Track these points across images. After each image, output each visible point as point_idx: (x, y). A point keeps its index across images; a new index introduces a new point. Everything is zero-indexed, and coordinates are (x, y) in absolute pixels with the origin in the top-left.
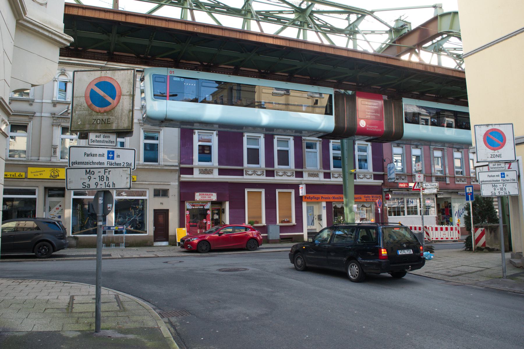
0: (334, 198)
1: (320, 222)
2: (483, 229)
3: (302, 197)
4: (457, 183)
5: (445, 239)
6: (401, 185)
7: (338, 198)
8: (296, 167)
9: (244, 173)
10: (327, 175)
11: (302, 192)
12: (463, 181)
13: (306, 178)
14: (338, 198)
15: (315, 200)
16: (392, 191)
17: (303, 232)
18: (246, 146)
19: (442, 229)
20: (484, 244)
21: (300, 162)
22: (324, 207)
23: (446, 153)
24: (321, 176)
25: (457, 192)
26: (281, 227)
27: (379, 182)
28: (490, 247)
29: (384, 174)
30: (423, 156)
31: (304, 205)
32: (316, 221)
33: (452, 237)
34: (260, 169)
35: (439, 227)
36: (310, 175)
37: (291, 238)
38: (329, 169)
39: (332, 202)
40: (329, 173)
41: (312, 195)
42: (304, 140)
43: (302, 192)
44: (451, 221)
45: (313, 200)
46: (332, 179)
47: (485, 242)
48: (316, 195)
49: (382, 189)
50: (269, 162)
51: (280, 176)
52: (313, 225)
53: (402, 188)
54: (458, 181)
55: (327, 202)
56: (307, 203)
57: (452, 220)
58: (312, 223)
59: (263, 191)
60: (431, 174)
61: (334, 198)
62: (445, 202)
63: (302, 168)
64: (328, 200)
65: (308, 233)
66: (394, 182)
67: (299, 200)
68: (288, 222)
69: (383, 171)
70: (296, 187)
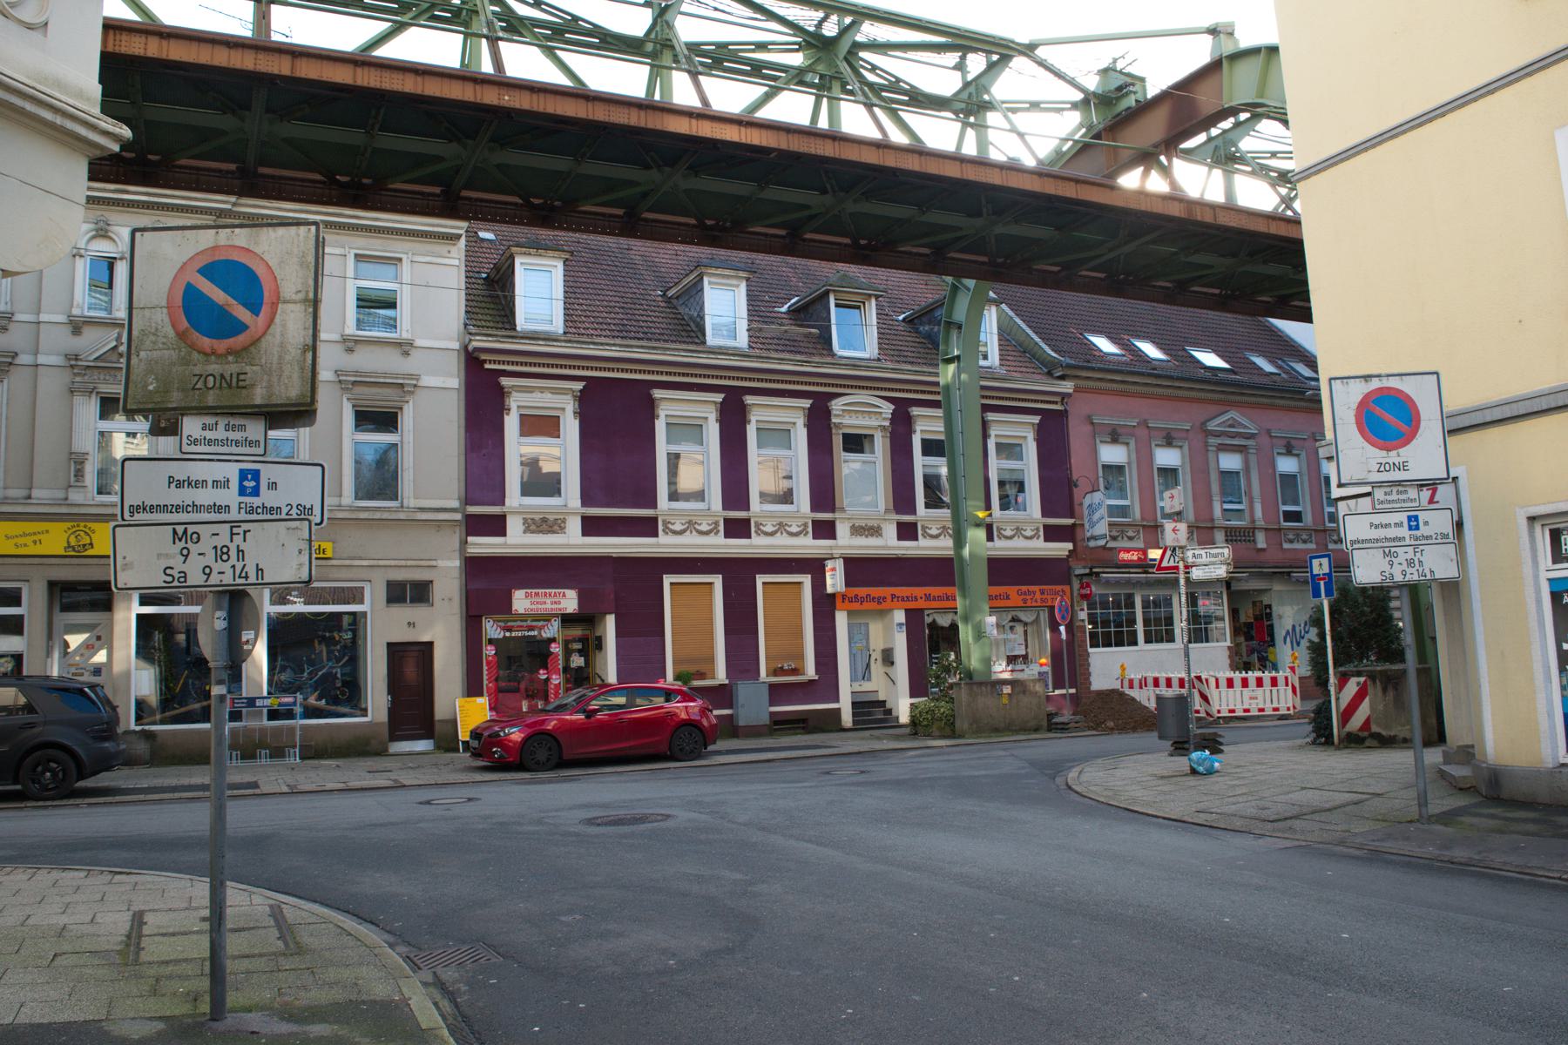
0: (928, 597)
2: (1362, 679)
3: (833, 596)
4: (1286, 546)
5: (1254, 713)
6: (1124, 556)
7: (940, 598)
8: (816, 505)
9: (660, 527)
10: (907, 531)
12: (1305, 542)
14: (940, 598)
17: (837, 700)
19: (1245, 683)
21: (824, 492)
22: (900, 625)
23: (1253, 459)
24: (890, 531)
25: (1289, 573)
27: (1061, 549)
31: (841, 619)
32: (877, 669)
33: (1275, 705)
35: (1237, 676)
36: (857, 531)
37: (804, 721)
38: (913, 511)
39: (922, 610)
40: (914, 525)
41: (862, 591)
42: (838, 426)
43: (835, 581)
44: (1271, 657)
45: (866, 606)
46: (923, 542)
49: (1070, 568)
51: (766, 534)
52: (869, 679)
53: (1127, 565)
54: (1291, 541)
55: (908, 611)
56: (850, 614)
58: (866, 674)
59: (717, 581)
60: (1212, 520)
63: (833, 510)
64: (912, 605)
67: (825, 606)
68: (795, 671)
69: (1072, 516)
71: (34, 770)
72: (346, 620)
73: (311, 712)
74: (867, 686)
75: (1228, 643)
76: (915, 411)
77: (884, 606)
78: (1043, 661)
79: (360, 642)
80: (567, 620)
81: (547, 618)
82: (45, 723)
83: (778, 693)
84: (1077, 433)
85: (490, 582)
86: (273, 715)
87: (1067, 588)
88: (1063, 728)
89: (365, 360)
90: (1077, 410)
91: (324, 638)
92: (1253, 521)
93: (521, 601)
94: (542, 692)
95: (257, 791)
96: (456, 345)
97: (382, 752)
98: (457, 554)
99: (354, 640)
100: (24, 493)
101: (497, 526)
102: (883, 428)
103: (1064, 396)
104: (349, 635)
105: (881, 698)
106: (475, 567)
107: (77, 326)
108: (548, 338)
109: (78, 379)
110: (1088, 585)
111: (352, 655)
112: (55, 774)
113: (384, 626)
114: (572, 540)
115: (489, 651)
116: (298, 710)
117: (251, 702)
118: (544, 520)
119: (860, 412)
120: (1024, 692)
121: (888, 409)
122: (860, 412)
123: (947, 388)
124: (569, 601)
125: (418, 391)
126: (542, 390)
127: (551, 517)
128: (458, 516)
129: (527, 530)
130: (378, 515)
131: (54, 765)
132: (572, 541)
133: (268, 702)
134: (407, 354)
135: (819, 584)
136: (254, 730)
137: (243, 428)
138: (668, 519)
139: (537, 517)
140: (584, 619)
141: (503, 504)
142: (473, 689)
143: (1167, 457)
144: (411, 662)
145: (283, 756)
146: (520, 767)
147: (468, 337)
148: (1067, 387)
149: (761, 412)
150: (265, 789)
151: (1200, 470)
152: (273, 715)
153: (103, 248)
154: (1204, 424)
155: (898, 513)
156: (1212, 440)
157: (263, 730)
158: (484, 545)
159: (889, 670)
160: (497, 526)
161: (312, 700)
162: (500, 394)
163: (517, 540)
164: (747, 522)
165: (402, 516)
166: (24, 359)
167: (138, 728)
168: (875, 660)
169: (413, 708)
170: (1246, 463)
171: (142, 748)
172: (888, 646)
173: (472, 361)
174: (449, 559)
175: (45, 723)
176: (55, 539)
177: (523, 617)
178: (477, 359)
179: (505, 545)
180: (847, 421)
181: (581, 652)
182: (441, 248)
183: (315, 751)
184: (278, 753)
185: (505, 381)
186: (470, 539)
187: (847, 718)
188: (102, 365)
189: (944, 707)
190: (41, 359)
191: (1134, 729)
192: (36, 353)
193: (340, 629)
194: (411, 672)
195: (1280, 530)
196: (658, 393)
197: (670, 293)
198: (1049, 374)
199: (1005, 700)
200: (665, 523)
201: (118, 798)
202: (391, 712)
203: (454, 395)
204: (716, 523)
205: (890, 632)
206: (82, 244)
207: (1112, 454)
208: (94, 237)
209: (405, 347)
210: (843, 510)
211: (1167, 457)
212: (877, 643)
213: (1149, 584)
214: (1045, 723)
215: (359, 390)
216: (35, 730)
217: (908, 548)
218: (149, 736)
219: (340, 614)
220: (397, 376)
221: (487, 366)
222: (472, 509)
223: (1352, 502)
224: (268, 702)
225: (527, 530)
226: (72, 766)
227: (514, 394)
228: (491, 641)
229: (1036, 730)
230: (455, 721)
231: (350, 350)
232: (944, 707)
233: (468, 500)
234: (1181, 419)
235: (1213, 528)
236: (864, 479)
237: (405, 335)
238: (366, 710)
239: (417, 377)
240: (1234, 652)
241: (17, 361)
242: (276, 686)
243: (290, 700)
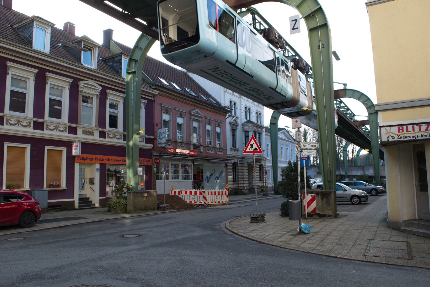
0: (108, 160)
1: (92, 186)
2: (313, 195)
3: (75, 156)
4: (207, 151)
5: (217, 203)
6: (170, 150)
7: (112, 160)
8: (70, 121)
9: (5, 121)
10: (102, 135)
11: (76, 151)
13: (80, 135)
14: (112, 160)
15: (89, 161)
16: (162, 156)
17: (73, 198)
18: (9, 88)
20: (314, 210)
22: (98, 169)
23: (201, 124)
24: (97, 134)
25: (209, 160)
26: (49, 192)
27: (150, 146)
28: (321, 213)
29: (154, 139)
30: (185, 124)
31: (77, 166)
32: (87, 186)
33: (212, 201)
34: (27, 118)
36: (85, 132)
37: (60, 206)
38: (105, 127)
39: (106, 164)
41: (85, 156)
42: (82, 91)
43: (76, 151)
44: (202, 185)
46: (107, 139)
47: (315, 208)
48: (90, 156)
49: (152, 153)
50: (39, 111)
51: (50, 130)
52: (84, 189)
53: (171, 153)
54: (208, 150)
55: (101, 164)
56: (80, 164)
57: (203, 184)
59: (28, 147)
60: (190, 142)
61: (108, 160)
62: (197, 168)
63: (77, 123)
64: (102, 162)
65: (80, 199)
66: (162, 147)
67: (71, 160)
69: (154, 136)
70: (69, 145)
74: (83, 192)
75: (192, 180)
76: (109, 91)
77: (93, 162)
78: (142, 184)
83: (51, 194)
84: (157, 108)
87: (150, 159)
88: (164, 208)
90: (158, 100)
92: (200, 143)
102: (97, 95)
103: (155, 95)
105: (88, 197)
110: (158, 159)
119: (90, 88)
120: (151, 196)
121: (99, 88)
122: (90, 88)
123: (128, 83)
135: (69, 151)
138: (9, 118)
143: (180, 120)
148: (156, 92)
149: (52, 81)
151: (189, 125)
154: (190, 112)
155: (100, 127)
156: (192, 117)
159: (92, 186)
164: (43, 124)
168: (88, 183)
170: (199, 125)
172: (92, 177)
180: (85, 90)
185: (48, 74)
187: (77, 205)
189: (123, 201)
191: (185, 209)
195: (206, 146)
196: (9, 64)
197: (14, 26)
198: (150, 87)
199: (145, 199)
200: (7, 120)
204: (30, 123)
205: (94, 172)
207: (166, 117)
210: (80, 124)
211: (180, 120)
212: (88, 176)
213: (173, 160)
214: (156, 207)
217: (102, 141)
223: (388, 128)
229: (154, 209)
232: (123, 201)
234: (185, 108)
235: (190, 144)
236: (90, 113)
240: (194, 183)
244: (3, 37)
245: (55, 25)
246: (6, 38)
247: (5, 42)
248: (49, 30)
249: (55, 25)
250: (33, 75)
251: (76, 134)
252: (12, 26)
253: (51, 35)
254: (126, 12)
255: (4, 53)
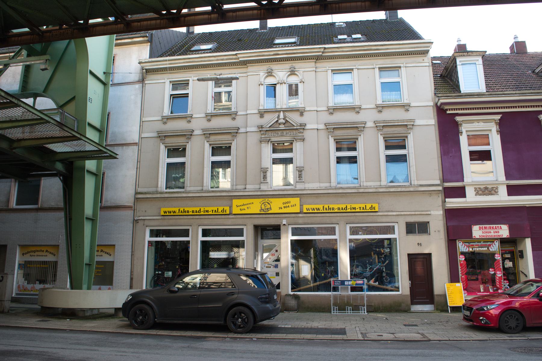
71: (234, 317)
72: (386, 243)
73: (371, 288)
79: (394, 253)
80: (503, 241)
81: (492, 240)
82: (238, 293)
85: (459, 223)
86: (353, 289)
89: (389, 115)
91: (376, 251)
93: (477, 232)
94: (493, 280)
95: (345, 337)
96: (431, 104)
97: (407, 311)
98: (441, 208)
99: (391, 253)
100: (243, 187)
101: (460, 192)
104: (388, 250)
106: (451, 214)
107: (262, 114)
108: (479, 95)
109: (263, 136)
111: (389, 261)
112: (243, 320)
113: (405, 246)
114: (502, 198)
115: (461, 258)
116: (365, 287)
117: (343, 282)
118: (486, 188)
124: (504, 231)
125: (414, 128)
126: (478, 121)
127: (490, 187)
128: (440, 188)
129: (477, 194)
130: (399, 189)
131: (243, 315)
132: (503, 199)
133: (350, 283)
134: (407, 110)
136: (344, 296)
137: (356, 284)
139: (482, 187)
140: (510, 244)
141: (463, 181)
142: (454, 279)
144: (420, 264)
145: (359, 310)
146: (498, 330)
147: (437, 99)
150: (350, 335)
152: (353, 289)
153: (271, 81)
157: (349, 297)
158: (454, 203)
160: (460, 192)
161: (371, 282)
162: (457, 125)
163: (472, 200)
165: (412, 189)
166: (242, 130)
167: (292, 293)
169: (422, 287)
171: (293, 303)
173: (440, 111)
174: (437, 210)
175: (238, 293)
176: (255, 206)
177: (479, 240)
178: (442, 109)
179: (466, 202)
181: (510, 259)
182: (419, 59)
183: (374, 308)
184: (356, 308)
185: (458, 119)
186: (447, 200)
188: (273, 129)
190: (249, 129)
192: (246, 127)
193: (383, 247)
194: (419, 269)
197: (537, 71)
201: (274, 336)
202: (411, 289)
203: (433, 127)
206: (262, 80)
208: (267, 77)
209: (406, 107)
215: (386, 130)
216: (235, 296)
218: (296, 297)
219: (382, 240)
220: (403, 121)
221: (448, 112)
222: (447, 185)
224: (350, 283)
225: (477, 194)
226: (251, 316)
227: (464, 125)
228: (462, 253)
230: (445, 295)
231: (380, 112)
233: (444, 180)
237: (406, 101)
238: (398, 288)
239: (413, 121)
241: (240, 131)
242: (354, 275)
243: (361, 282)
244: (528, 88)
245: (486, 52)
246: (531, 88)
247: (531, 93)
248: (480, 60)
249: (486, 52)
250: (493, 123)
251: (464, 196)
252: (533, 72)
253: (484, 65)
254: (185, 11)
255: (534, 106)
